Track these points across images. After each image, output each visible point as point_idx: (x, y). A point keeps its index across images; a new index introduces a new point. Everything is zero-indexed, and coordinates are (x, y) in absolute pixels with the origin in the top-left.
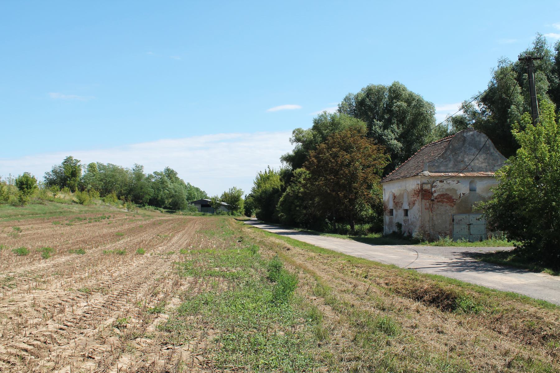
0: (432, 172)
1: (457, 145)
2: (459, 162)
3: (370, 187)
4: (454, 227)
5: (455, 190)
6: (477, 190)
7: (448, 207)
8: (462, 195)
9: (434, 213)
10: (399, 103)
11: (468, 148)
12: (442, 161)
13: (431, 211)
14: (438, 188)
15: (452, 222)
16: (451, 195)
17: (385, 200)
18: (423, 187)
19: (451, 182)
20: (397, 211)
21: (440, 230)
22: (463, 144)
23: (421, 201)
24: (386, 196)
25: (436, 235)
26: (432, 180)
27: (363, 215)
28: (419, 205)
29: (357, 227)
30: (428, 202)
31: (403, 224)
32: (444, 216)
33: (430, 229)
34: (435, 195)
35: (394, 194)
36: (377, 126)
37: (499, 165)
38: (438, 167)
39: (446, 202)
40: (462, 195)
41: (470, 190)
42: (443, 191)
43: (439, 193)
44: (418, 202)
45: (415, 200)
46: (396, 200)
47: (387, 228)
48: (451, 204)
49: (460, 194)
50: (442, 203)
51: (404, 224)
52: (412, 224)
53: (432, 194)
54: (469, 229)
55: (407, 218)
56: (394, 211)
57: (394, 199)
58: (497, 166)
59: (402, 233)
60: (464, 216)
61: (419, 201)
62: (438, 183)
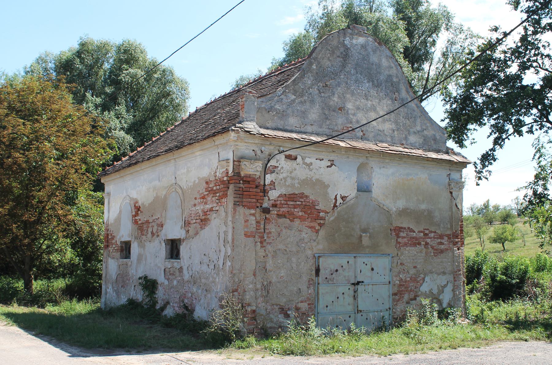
0: (268, 128)
1: (328, 63)
2: (334, 111)
3: (71, 201)
4: (320, 292)
5: (321, 185)
6: (373, 191)
7: (306, 234)
8: (339, 200)
9: (269, 247)
10: (131, 70)
11: (354, 77)
12: (293, 101)
13: (261, 243)
14: (281, 176)
15: (314, 277)
16: (312, 197)
17: (108, 220)
18: (243, 167)
19: (313, 160)
20: (142, 245)
21: (283, 301)
22: (344, 66)
23: (235, 210)
24: (112, 210)
25: (271, 316)
26: (268, 149)
27: (53, 261)
28: (226, 224)
29: (37, 285)
30: (253, 215)
31: (161, 279)
32: (294, 260)
33: (256, 298)
34: (273, 194)
35: (137, 202)
36: (90, 105)
37: (418, 132)
38: (283, 115)
39: (300, 218)
40: (339, 200)
41: (358, 190)
42: (293, 185)
43: (283, 191)
44: (223, 214)
45: (211, 210)
46: (142, 218)
47: (110, 290)
48: (312, 224)
49: (336, 199)
50: (291, 221)
51: (166, 282)
52: (194, 281)
53: (265, 192)
54: (355, 298)
55: (176, 263)
56: (135, 249)
57: (137, 214)
58: (415, 133)
59: (158, 307)
60: (342, 260)
61: (226, 212)
62: (281, 161)
